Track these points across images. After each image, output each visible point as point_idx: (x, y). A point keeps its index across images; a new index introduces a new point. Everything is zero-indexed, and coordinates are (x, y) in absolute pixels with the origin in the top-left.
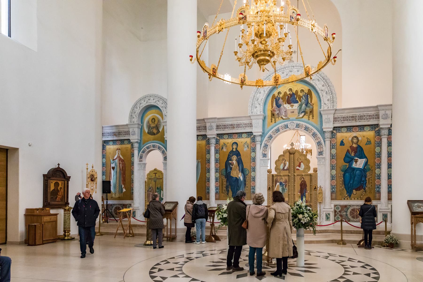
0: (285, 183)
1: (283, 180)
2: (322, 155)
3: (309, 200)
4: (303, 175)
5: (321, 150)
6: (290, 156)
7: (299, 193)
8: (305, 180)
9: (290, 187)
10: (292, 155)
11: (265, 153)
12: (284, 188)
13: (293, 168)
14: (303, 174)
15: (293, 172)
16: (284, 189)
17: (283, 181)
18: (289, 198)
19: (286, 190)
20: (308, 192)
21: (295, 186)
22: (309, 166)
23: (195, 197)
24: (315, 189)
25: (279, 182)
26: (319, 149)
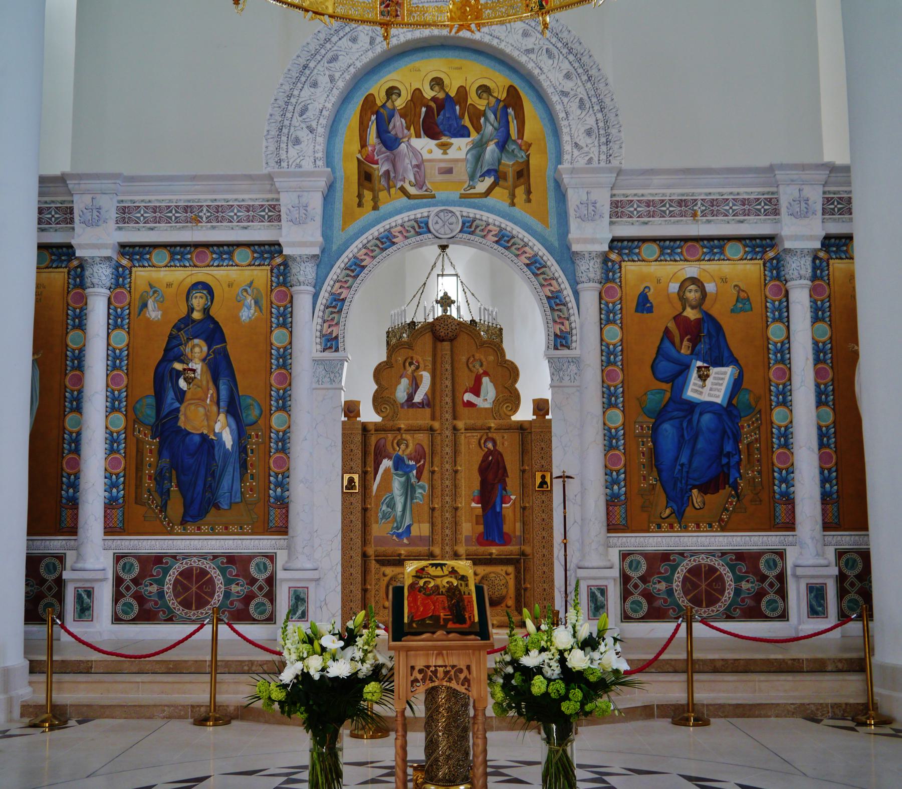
0: (417, 462)
1: (407, 446)
2: (569, 348)
3: (518, 533)
4: (489, 428)
7: (473, 505)
8: (500, 448)
9: (436, 476)
10: (445, 343)
12: (413, 480)
13: (448, 400)
14: (492, 425)
15: (448, 416)
16: (412, 485)
17: (408, 451)
18: (433, 525)
19: (420, 491)
20: (513, 497)
21: (459, 476)
22: (516, 389)
24: (541, 485)
25: (390, 458)
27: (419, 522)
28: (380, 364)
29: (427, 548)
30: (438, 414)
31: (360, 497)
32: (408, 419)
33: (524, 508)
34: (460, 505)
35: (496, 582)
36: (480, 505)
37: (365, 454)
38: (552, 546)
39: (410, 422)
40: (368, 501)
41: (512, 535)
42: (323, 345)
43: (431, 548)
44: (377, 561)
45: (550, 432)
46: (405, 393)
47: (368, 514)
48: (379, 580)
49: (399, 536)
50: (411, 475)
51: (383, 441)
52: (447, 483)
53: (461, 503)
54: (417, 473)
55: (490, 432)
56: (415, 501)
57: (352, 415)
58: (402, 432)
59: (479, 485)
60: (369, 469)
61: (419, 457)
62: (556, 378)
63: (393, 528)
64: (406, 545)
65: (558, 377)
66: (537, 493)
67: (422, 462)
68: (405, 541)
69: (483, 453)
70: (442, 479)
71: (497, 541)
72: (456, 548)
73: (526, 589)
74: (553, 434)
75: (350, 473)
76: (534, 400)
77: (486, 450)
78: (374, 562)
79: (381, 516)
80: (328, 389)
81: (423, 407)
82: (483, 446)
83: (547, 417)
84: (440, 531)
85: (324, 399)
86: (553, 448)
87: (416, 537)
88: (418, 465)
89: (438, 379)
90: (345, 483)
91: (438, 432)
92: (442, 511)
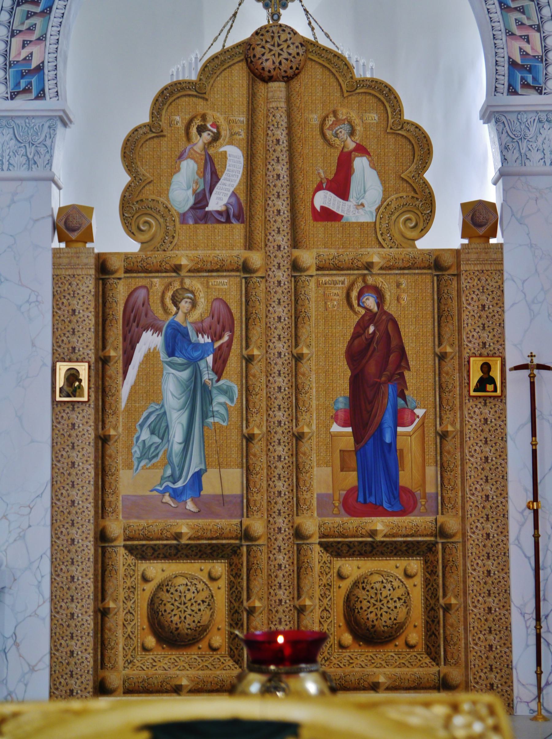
0: (216, 337)
1: (194, 304)
2: (539, 90)
3: (430, 489)
4: (369, 266)
5: (528, 48)
6: (261, 101)
7: (336, 428)
8: (391, 307)
9: (256, 368)
10: (274, 85)
11: (28, 59)
12: (208, 376)
13: (282, 205)
14: (376, 259)
15: (283, 240)
16: (204, 386)
17: (196, 315)
18: (249, 471)
19: (222, 399)
20: (420, 412)
21: (304, 367)
22: (426, 184)
23: (209, 205)
24: (482, 385)
25: (157, 329)
26: (510, 34)
27: (220, 465)
28: (136, 130)
29: (237, 521)
30: (259, 236)
31: (92, 411)
32: (196, 248)
33: (443, 436)
34: (306, 430)
35: (385, 593)
36: (350, 429)
37: (104, 321)
38: (505, 516)
39: (200, 253)
40: (111, 420)
41: (418, 493)
42: (11, 84)
43: (246, 522)
44: (130, 550)
45: (501, 272)
46: (190, 192)
47: (111, 449)
48: (132, 589)
49: (176, 494)
50: (202, 364)
51: (142, 293)
52: (280, 381)
53: (309, 425)
54: (215, 361)
55: (372, 274)
56: (211, 420)
57: (74, 236)
58: (183, 273)
59: (347, 385)
60: (112, 353)
61: (219, 328)
62: (512, 156)
63: (163, 479)
64: (193, 515)
65: (516, 154)
66: (471, 403)
67: (226, 338)
68: (190, 506)
69: (356, 319)
70: (268, 374)
71: (385, 505)
72: (298, 520)
73: (447, 608)
74: (506, 276)
75: (70, 361)
76: (464, 206)
77: (363, 312)
78: (122, 551)
79: (138, 454)
80: (21, 180)
81: (228, 221)
82: (355, 303)
83: (492, 241)
84: (265, 485)
85: (13, 202)
86: (507, 306)
87: (214, 497)
88: (217, 344)
89: (259, 162)
90: (60, 382)
91: (259, 274)
92: (269, 443)
